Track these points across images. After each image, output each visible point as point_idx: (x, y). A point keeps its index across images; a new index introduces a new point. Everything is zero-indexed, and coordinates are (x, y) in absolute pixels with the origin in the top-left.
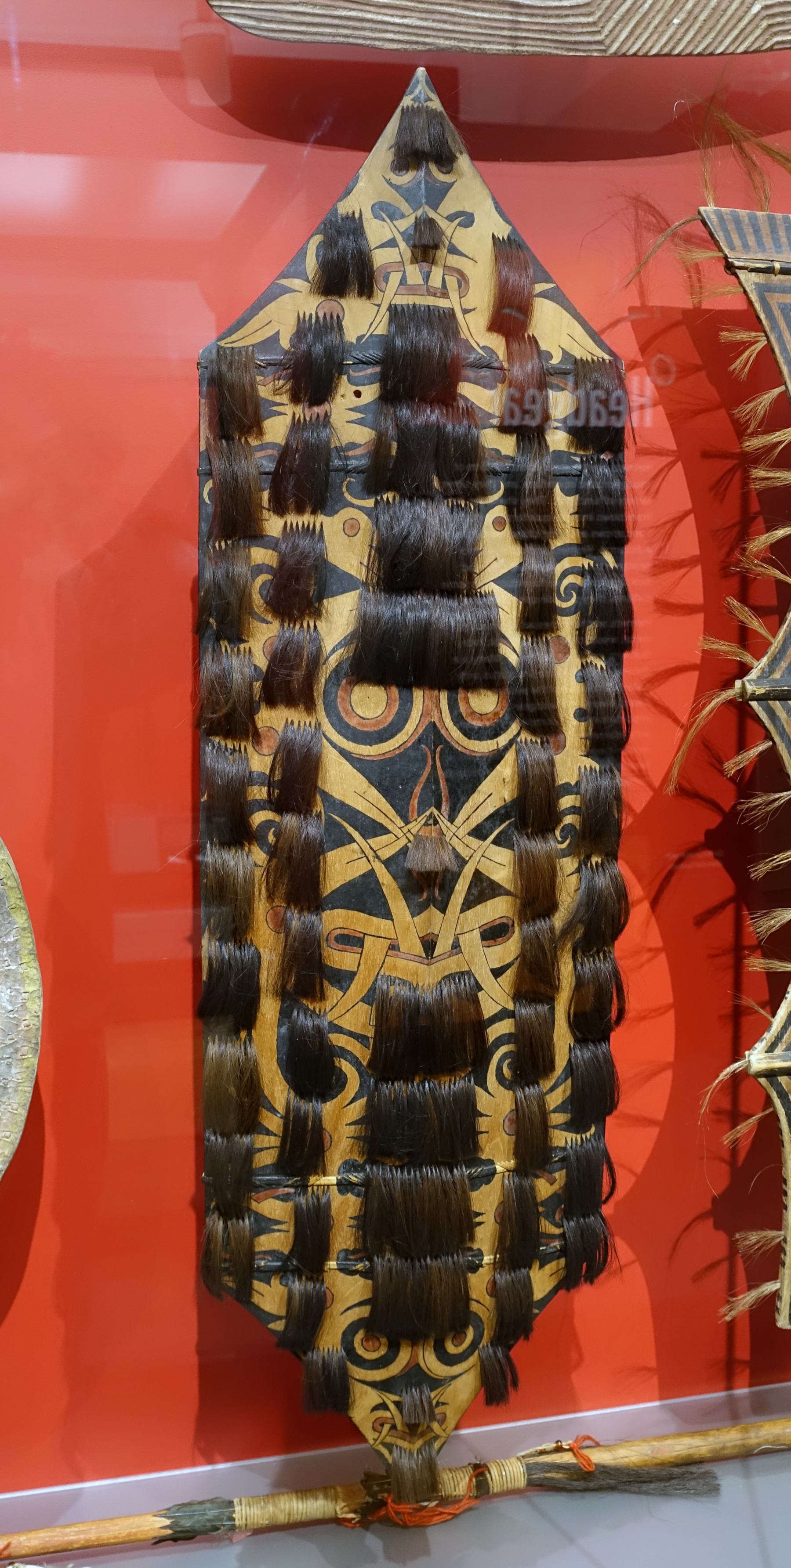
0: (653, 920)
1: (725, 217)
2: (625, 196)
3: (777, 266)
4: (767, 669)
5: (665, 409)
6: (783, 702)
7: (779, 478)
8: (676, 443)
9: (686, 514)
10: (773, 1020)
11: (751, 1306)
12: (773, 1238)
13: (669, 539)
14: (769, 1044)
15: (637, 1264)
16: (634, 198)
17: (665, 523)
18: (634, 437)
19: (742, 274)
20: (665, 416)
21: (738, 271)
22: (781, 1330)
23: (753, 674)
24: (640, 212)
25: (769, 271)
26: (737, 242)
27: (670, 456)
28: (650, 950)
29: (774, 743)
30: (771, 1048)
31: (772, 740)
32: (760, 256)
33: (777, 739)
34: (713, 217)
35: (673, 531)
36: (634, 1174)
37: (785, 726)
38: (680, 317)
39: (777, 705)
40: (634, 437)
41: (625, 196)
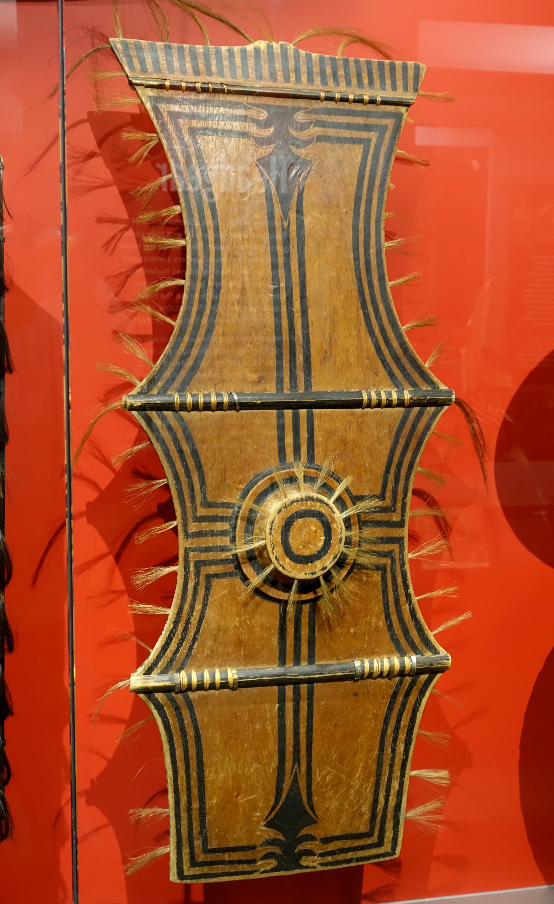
0: (117, 570)
1: (129, 46)
2: (83, 28)
3: (167, 83)
4: (146, 387)
5: (118, 188)
6: (159, 412)
7: (164, 243)
8: (128, 213)
9: (137, 267)
10: (151, 650)
11: (147, 865)
12: (160, 814)
13: (123, 287)
14: (147, 669)
15: (110, 829)
16: (91, 30)
17: (120, 274)
18: (9, 213)
19: (139, 90)
20: (118, 193)
21: (136, 87)
22: (172, 883)
23: (134, 392)
24: (95, 40)
25: (161, 87)
26: (137, 66)
27: (123, 223)
28: (115, 592)
29: (151, 442)
30: (148, 672)
31: (150, 440)
32: (155, 76)
33: (153, 440)
34: (119, 46)
35: (127, 280)
36: (106, 758)
37: (160, 430)
38: (129, 120)
39: (153, 414)
40: (9, 213)
41: (83, 28)
